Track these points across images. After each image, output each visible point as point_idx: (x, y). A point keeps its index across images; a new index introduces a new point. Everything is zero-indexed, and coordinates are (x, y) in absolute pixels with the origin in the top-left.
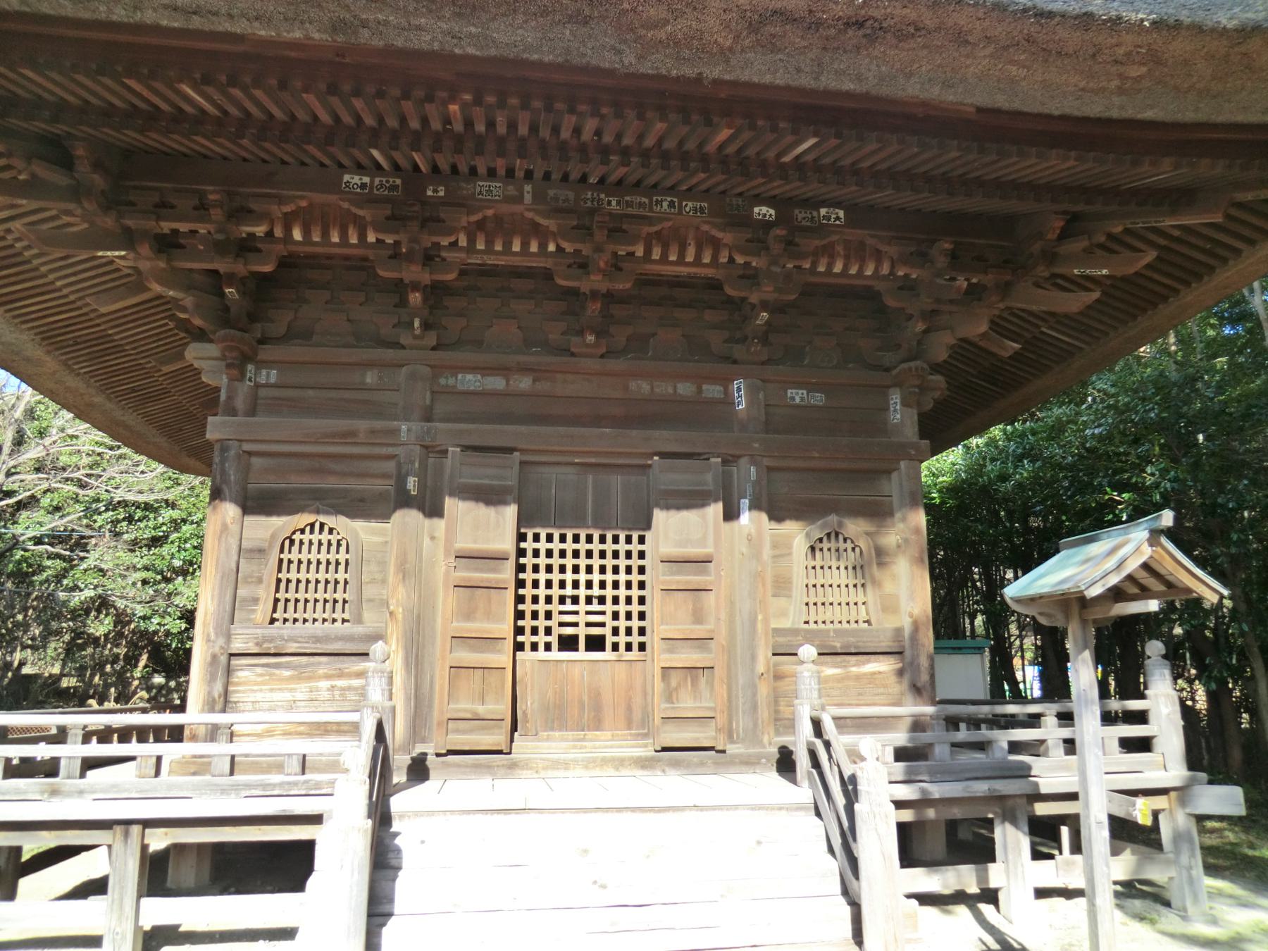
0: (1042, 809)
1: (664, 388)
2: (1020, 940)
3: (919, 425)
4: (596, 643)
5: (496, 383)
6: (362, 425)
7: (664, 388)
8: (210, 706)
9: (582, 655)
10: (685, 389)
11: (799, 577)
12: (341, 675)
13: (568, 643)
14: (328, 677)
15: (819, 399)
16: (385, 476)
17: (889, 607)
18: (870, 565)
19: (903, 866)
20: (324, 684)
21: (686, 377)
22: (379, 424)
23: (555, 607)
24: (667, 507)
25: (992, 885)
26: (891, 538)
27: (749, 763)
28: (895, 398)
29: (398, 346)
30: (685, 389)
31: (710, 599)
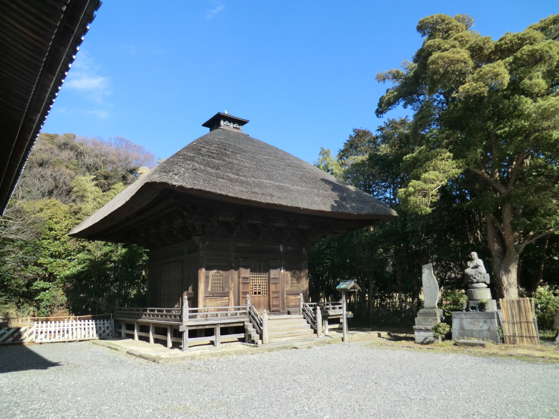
0: (329, 318)
3: (141, 188)
4: (259, 293)
5: (244, 245)
9: (257, 295)
11: (290, 281)
12: (222, 300)
13: (255, 293)
15: (292, 249)
17: (302, 287)
18: (299, 279)
24: (273, 269)
25: (495, 301)
26: (302, 274)
27: (283, 313)
28: (304, 249)
31: (278, 285)
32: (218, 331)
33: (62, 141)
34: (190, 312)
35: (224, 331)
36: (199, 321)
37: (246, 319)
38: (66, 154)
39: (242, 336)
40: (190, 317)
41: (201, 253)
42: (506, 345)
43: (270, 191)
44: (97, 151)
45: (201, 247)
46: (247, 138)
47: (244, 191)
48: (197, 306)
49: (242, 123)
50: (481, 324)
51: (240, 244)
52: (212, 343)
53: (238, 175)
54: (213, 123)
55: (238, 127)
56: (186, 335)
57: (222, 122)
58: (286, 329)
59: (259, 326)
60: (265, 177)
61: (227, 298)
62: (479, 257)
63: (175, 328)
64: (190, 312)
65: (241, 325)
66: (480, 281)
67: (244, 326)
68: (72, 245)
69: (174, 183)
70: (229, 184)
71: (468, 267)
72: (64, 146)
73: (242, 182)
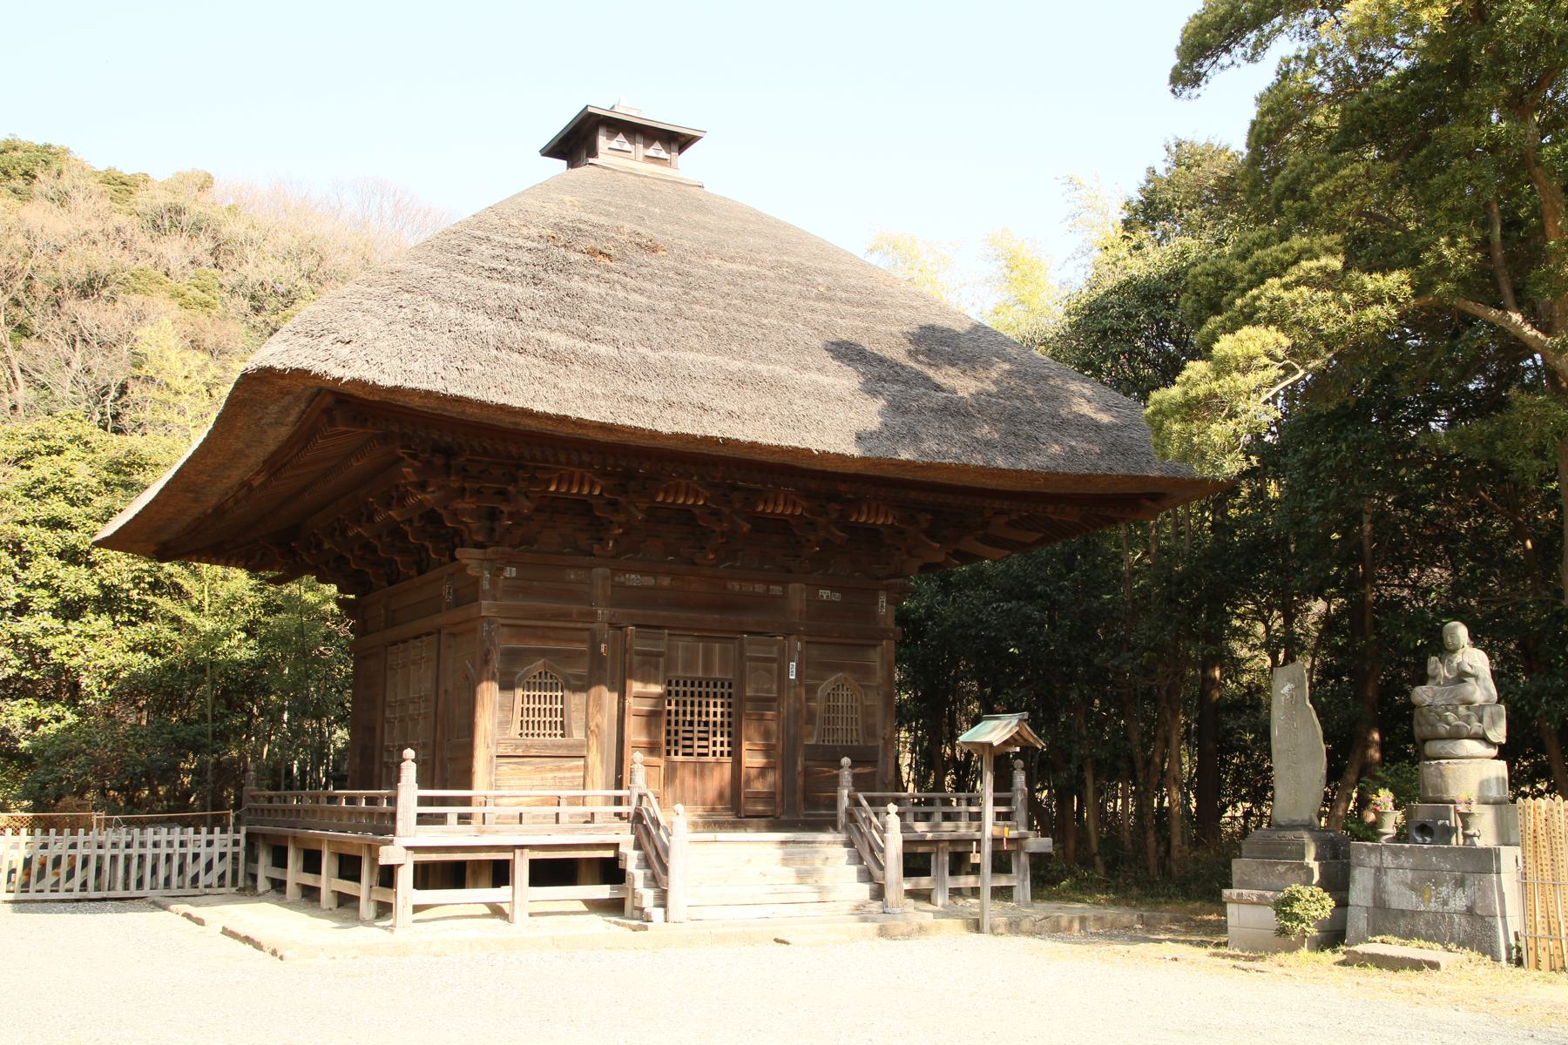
1: (748, 587)
2: (916, 945)
5: (649, 581)
6: (575, 608)
7: (748, 587)
8: (491, 786)
10: (760, 588)
12: (559, 769)
14: (551, 770)
15: (837, 597)
16: (582, 641)
19: (415, 887)
20: (550, 775)
21: (759, 581)
22: (585, 608)
23: (681, 728)
29: (591, 554)
30: (760, 588)
32: (521, 872)
33: (164, 199)
34: (423, 801)
35: (550, 872)
36: (451, 836)
37: (624, 837)
38: (173, 249)
39: (603, 892)
40: (422, 819)
41: (486, 607)
42: (1542, 973)
43: (699, 394)
44: (288, 236)
45: (486, 585)
46: (692, 198)
47: (593, 396)
48: (469, 786)
49: (678, 141)
50: (1444, 890)
51: (634, 579)
52: (497, 911)
53: (586, 337)
54: (574, 144)
55: (663, 154)
56: (405, 877)
57: (603, 142)
58: (731, 875)
59: (657, 864)
60: (694, 342)
61: (581, 762)
62: (1476, 640)
63: (314, 847)
64: (423, 801)
65: (610, 854)
66: (1465, 733)
67: (616, 860)
68: (120, 568)
69: (337, 373)
70: (541, 367)
71: (1423, 679)
72: (167, 221)
73: (594, 362)
